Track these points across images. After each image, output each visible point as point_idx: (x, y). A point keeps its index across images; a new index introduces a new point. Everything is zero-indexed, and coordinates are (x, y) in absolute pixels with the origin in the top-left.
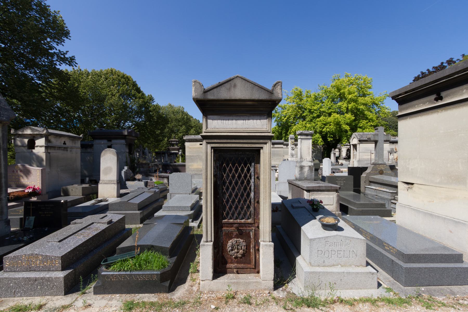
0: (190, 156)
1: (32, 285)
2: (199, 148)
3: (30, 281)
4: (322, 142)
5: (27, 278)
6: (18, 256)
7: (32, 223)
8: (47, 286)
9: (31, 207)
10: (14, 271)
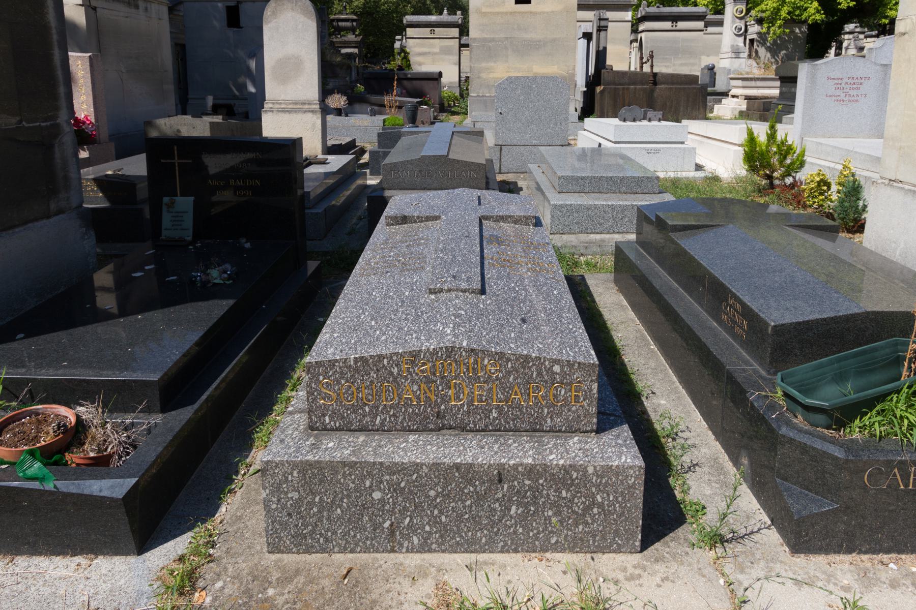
0: (485, 40)
1: (480, 498)
2: (512, 13)
3: (470, 482)
4: (818, 12)
5: (457, 467)
6: (381, 357)
7: (189, 221)
8: (555, 506)
9: (176, 161)
10: (362, 429)
